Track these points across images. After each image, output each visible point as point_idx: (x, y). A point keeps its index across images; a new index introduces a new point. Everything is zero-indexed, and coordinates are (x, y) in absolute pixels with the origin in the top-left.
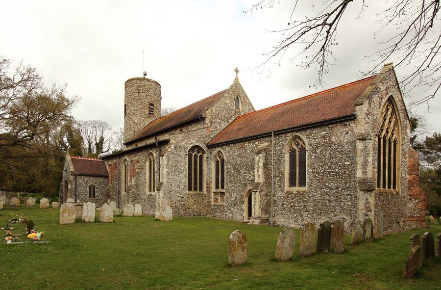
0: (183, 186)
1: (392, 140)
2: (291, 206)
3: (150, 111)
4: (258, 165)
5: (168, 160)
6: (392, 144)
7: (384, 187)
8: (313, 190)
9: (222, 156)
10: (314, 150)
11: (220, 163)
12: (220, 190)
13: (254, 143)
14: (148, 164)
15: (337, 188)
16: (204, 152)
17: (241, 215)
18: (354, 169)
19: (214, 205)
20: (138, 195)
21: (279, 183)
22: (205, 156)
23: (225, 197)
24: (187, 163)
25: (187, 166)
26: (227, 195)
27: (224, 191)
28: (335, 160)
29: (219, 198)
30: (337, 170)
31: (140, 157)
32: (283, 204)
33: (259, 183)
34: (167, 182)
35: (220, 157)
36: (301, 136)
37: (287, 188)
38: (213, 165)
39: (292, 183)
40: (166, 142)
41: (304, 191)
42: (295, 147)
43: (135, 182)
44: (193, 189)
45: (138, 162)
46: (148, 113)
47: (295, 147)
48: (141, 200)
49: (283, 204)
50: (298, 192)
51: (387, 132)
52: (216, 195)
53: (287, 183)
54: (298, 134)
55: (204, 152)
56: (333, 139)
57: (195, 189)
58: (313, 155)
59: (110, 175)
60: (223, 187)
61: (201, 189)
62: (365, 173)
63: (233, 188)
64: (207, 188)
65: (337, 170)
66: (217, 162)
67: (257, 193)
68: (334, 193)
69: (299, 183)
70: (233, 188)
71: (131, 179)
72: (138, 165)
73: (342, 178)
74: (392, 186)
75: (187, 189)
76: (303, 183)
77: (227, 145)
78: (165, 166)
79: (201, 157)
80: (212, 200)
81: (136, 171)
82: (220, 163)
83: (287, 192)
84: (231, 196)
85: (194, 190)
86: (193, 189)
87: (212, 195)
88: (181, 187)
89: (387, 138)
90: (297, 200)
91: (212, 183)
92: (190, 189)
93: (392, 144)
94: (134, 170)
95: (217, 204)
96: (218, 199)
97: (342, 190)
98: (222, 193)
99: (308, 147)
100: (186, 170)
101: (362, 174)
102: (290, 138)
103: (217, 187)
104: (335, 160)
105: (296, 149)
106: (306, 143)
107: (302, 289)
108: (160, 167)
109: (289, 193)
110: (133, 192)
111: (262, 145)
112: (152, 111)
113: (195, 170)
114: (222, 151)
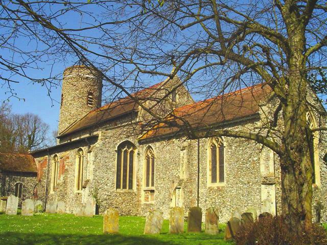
0: (111, 184)
2: (212, 203)
3: (88, 100)
4: (183, 161)
5: (96, 156)
8: (230, 185)
11: (218, 150)
12: (150, 188)
14: (77, 160)
15: (249, 183)
16: (134, 147)
19: (145, 204)
20: (66, 194)
21: (202, 180)
22: (136, 151)
23: (155, 195)
24: (116, 160)
25: (116, 162)
26: (156, 193)
27: (153, 188)
29: (150, 197)
30: (248, 165)
31: (72, 153)
32: (206, 201)
34: (94, 179)
35: (151, 153)
37: (209, 184)
38: (143, 163)
39: (214, 180)
40: (95, 139)
41: (223, 187)
43: (64, 180)
45: (68, 158)
48: (69, 200)
49: (206, 201)
50: (218, 188)
52: (146, 193)
53: (209, 178)
54: (150, 145)
55: (134, 147)
57: (124, 187)
58: (230, 151)
59: (39, 173)
60: (153, 185)
61: (131, 187)
62: (267, 167)
63: (162, 185)
64: (138, 185)
65: (248, 165)
67: (180, 190)
68: (246, 188)
69: (220, 179)
70: (162, 185)
71: (60, 176)
72: (67, 161)
73: (252, 173)
75: (115, 186)
76: (222, 179)
78: (92, 162)
79: (132, 152)
80: (142, 199)
81: (66, 168)
82: (218, 150)
83: (209, 188)
84: (160, 194)
85: (123, 188)
86: (122, 187)
87: (143, 193)
88: (108, 184)
90: (217, 196)
91: (143, 179)
92: (118, 186)
94: (64, 166)
95: (148, 203)
96: (148, 198)
97: (253, 184)
98: (152, 191)
99: (225, 144)
100: (114, 166)
101: (265, 169)
103: (148, 185)
105: (216, 145)
108: (87, 163)
109: (211, 189)
110: (61, 191)
112: (90, 101)
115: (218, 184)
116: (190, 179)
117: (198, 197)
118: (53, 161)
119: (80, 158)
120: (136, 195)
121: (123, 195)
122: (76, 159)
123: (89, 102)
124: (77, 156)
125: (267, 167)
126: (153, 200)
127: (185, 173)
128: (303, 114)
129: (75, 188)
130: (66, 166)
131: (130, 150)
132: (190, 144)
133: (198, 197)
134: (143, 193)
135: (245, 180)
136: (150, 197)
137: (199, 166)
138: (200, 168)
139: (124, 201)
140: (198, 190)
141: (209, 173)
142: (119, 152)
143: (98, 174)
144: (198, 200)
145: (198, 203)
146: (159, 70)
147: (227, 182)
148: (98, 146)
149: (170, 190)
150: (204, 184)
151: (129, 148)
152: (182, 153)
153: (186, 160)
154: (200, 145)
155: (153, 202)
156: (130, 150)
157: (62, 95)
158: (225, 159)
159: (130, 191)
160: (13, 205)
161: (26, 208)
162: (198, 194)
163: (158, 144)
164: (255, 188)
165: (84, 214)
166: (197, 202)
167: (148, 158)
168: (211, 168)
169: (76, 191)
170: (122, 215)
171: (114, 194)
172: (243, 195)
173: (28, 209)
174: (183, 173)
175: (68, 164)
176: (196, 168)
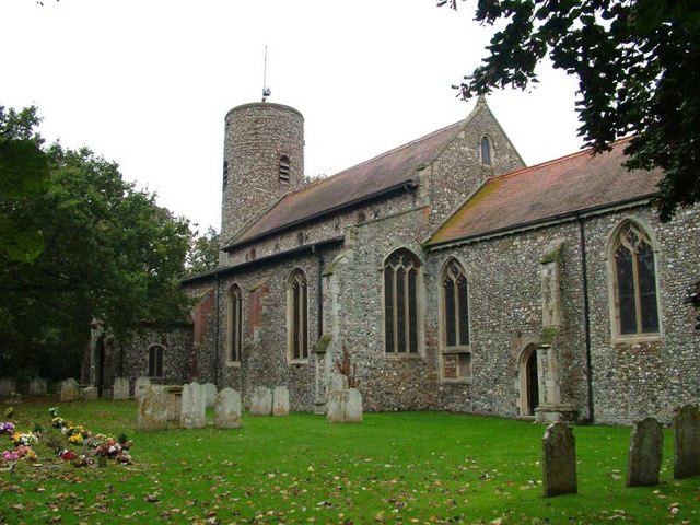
5: (342, 284)
9: (460, 271)
12: (458, 347)
14: (289, 294)
16: (418, 263)
19: (446, 384)
22: (421, 271)
23: (471, 364)
29: (458, 368)
32: (610, 375)
34: (341, 334)
35: (456, 273)
36: (640, 221)
37: (616, 337)
39: (627, 326)
49: (610, 375)
50: (643, 344)
52: (449, 359)
54: (633, 217)
55: (418, 263)
58: (671, 260)
60: (465, 341)
61: (414, 349)
63: (490, 342)
67: (549, 351)
70: (490, 342)
76: (650, 324)
79: (413, 273)
80: (441, 373)
84: (486, 360)
90: (642, 363)
92: (390, 348)
95: (452, 380)
98: (465, 356)
99: (656, 245)
100: (380, 304)
103: (451, 341)
105: (454, 280)
106: (653, 237)
109: (621, 347)
110: (256, 360)
114: (460, 259)
115: (636, 339)
116: (567, 329)
117: (589, 366)
118: (228, 299)
119: (234, 302)
120: (425, 364)
121: (400, 366)
122: (288, 292)
124: (290, 285)
126: (469, 375)
127: (555, 313)
129: (289, 354)
130: (265, 308)
131: (398, 266)
133: (589, 366)
134: (440, 359)
136: (458, 368)
137: (586, 298)
138: (591, 302)
139: (403, 377)
140: (589, 353)
141: (613, 312)
142: (388, 272)
143: (348, 322)
144: (590, 374)
145: (590, 380)
147: (667, 333)
148: (344, 261)
150: (606, 340)
151: (406, 265)
152: (543, 272)
153: (554, 287)
154: (587, 249)
155: (469, 379)
158: (657, 282)
159: (412, 356)
160: (194, 404)
161: (224, 409)
162: (589, 359)
163: (473, 254)
165: (345, 416)
166: (585, 377)
167: (449, 285)
168: (618, 301)
169: (291, 361)
170: (399, 410)
171: (382, 364)
173: (228, 412)
174: (551, 314)
175: (267, 303)
176: (578, 302)
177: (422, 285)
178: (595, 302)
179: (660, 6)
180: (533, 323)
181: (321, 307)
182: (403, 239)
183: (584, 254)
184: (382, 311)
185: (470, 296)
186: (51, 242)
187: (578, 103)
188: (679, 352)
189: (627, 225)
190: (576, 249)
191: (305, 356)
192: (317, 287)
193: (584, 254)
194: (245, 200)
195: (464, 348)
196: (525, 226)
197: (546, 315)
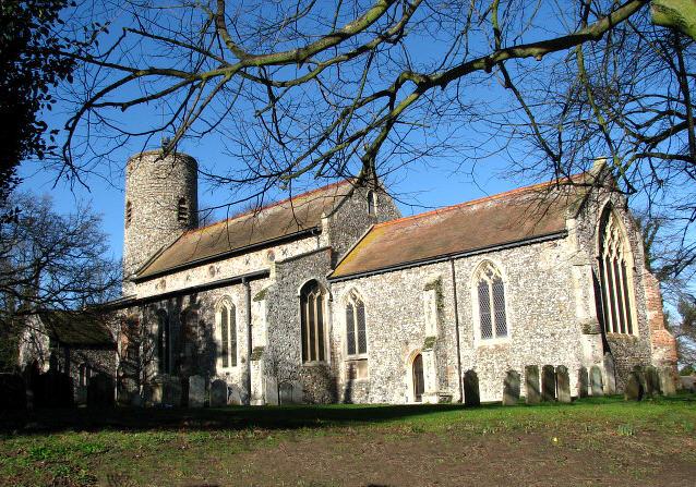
1: (619, 262)
5: (270, 307)
6: (620, 267)
7: (623, 331)
9: (358, 296)
10: (515, 282)
13: (418, 273)
17: (402, 395)
18: (573, 307)
28: (546, 295)
33: (262, 349)
36: (494, 261)
37: (479, 341)
39: (486, 332)
42: (486, 278)
44: (494, 332)
46: (175, 217)
47: (486, 278)
50: (497, 346)
51: (611, 251)
56: (541, 265)
62: (587, 309)
63: (383, 350)
66: (350, 307)
70: (383, 350)
74: (355, 310)
76: (502, 331)
77: (368, 276)
86: (494, 332)
89: (612, 260)
91: (342, 344)
93: (620, 267)
99: (505, 278)
102: (476, 264)
104: (546, 295)
106: (503, 272)
107: (694, 71)
109: (482, 349)
111: (431, 275)
113: (312, 323)
114: (359, 288)
123: (181, 211)
125: (587, 309)
128: (160, 330)
131: (318, 294)
132: (276, 363)
135: (547, 331)
146: (599, 382)
149: (402, 356)
150: (471, 346)
154: (457, 280)
156: (318, 294)
157: (129, 204)
164: (565, 342)
172: (543, 354)
177: (326, 307)
178: (463, 318)
179: (266, 147)
180: (417, 335)
181: (250, 327)
182: (312, 273)
183: (455, 284)
184: (298, 328)
185: (367, 315)
186: (286, 175)
187: (104, 249)
188: (520, 350)
189: (484, 264)
190: (447, 281)
191: (234, 365)
192: (245, 310)
193: (455, 284)
194: (149, 236)
195: (363, 356)
196: (542, 236)
197: (428, 326)
